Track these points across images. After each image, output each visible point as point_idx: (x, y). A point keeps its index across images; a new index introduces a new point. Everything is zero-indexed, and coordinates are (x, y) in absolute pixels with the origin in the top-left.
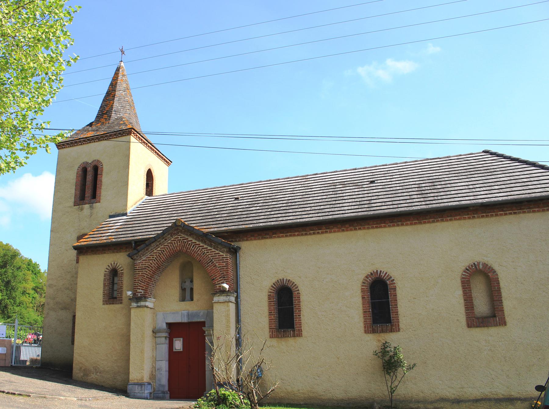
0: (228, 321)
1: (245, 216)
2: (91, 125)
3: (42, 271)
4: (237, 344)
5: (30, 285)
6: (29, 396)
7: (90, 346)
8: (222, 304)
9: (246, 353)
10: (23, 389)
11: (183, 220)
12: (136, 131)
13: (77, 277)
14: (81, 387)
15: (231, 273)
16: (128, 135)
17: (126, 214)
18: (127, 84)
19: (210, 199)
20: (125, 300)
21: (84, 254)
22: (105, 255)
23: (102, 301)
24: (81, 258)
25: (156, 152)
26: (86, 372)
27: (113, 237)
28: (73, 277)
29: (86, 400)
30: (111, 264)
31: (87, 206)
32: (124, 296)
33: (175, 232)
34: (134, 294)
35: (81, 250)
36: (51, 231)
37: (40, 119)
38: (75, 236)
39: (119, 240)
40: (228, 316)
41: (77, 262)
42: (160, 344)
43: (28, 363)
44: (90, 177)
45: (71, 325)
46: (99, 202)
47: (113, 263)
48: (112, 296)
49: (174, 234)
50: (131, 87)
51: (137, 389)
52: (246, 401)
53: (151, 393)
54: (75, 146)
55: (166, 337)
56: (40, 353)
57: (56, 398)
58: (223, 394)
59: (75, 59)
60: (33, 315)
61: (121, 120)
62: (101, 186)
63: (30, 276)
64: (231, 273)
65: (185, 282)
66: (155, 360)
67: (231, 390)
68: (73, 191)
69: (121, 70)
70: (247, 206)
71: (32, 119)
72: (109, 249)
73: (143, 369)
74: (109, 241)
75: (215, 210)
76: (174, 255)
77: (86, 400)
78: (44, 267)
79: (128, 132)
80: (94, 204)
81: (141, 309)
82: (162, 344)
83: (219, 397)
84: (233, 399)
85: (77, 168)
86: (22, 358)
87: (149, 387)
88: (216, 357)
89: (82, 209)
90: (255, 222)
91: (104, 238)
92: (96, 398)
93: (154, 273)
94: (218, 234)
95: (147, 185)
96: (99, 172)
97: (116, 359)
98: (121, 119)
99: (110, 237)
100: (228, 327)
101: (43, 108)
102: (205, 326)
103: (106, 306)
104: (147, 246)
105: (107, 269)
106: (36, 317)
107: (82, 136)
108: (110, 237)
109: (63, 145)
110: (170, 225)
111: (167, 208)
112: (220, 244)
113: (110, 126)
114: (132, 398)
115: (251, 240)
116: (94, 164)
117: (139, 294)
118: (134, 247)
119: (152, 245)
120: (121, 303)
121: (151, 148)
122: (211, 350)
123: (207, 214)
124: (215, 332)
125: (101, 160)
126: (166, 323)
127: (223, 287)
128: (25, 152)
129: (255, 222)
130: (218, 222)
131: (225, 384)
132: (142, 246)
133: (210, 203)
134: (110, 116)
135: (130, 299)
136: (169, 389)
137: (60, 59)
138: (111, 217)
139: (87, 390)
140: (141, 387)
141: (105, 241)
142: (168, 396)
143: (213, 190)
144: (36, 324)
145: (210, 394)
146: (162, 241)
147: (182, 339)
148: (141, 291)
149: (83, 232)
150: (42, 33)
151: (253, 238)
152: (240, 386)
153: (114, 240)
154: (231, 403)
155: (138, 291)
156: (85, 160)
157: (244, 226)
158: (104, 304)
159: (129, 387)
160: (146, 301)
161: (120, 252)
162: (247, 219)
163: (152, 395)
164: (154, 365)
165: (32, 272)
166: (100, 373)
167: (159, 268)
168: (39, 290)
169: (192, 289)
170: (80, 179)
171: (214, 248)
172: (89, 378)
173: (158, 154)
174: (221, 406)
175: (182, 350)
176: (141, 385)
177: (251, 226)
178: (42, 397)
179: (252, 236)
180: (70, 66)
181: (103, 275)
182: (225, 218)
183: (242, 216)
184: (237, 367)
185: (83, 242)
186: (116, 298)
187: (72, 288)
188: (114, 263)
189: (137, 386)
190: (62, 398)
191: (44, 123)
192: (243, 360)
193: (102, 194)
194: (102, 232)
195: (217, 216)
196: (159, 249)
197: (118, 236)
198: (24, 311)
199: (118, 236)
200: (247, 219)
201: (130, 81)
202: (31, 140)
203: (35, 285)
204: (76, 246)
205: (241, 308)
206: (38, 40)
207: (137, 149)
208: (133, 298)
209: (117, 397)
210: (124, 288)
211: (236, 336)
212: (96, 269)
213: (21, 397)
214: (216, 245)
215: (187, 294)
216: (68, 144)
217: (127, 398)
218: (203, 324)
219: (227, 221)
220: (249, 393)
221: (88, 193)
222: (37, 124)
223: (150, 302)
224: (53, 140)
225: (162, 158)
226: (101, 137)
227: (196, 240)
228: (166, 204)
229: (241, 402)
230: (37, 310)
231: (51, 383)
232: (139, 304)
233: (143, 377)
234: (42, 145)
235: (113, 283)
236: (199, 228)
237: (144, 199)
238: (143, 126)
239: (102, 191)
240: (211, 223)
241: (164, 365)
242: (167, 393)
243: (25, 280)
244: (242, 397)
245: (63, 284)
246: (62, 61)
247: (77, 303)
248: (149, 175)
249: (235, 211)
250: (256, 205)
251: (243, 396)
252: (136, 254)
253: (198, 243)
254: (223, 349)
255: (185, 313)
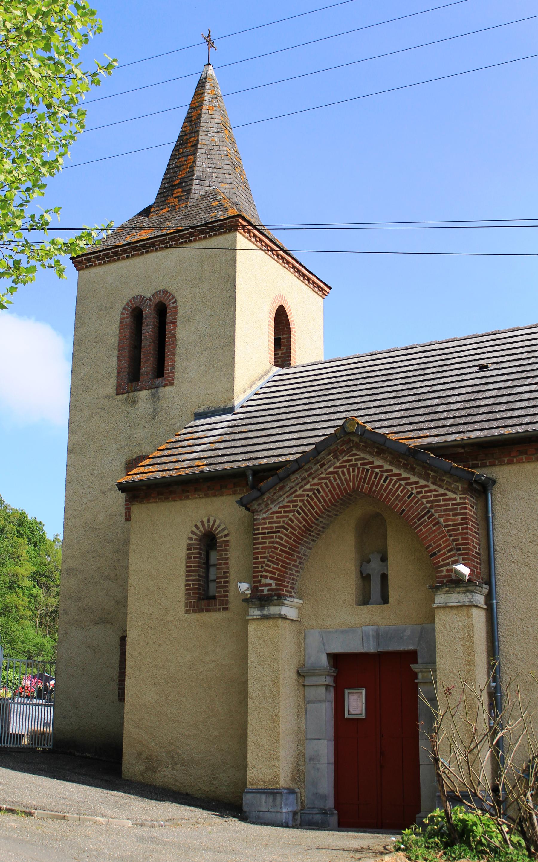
0: (470, 651)
1: (504, 407)
2: (146, 212)
3: (50, 536)
4: (491, 705)
5: (26, 569)
6: (31, 814)
7: (155, 710)
8: (455, 611)
9: (513, 725)
10: (18, 799)
11: (360, 420)
12: (250, 224)
13: (127, 553)
14: (141, 796)
15: (475, 539)
16: (230, 231)
17: (230, 410)
18: (223, 116)
19: (421, 369)
20: (235, 603)
21: (142, 502)
22: (188, 502)
23: (183, 605)
24: (137, 510)
25: (294, 267)
26: (152, 763)
27: (205, 462)
28: (118, 551)
29: (152, 826)
30: (202, 522)
31: (144, 394)
32: (231, 594)
33: (344, 447)
34: (254, 589)
35: (136, 493)
36: (69, 451)
37: (38, 204)
38: (120, 461)
39: (219, 467)
40: (469, 637)
41: (128, 518)
42: (314, 702)
43: (25, 741)
44: (149, 330)
45: (116, 658)
46: (172, 384)
47: (205, 520)
48: (205, 593)
49: (342, 452)
50: (233, 121)
51: (264, 804)
52: (515, 839)
53: (295, 813)
54: (114, 261)
55: (327, 686)
56: (50, 719)
57: (87, 820)
58: (460, 820)
59: (108, 67)
60: (31, 635)
61: (214, 199)
62: (174, 348)
63: (25, 550)
64: (475, 539)
65: (369, 561)
66: (303, 738)
67: (479, 812)
68: (114, 362)
69: (208, 86)
70: (509, 384)
71: (21, 205)
72: (196, 490)
73: (277, 759)
74: (197, 470)
75: (433, 395)
76: (344, 500)
77: (152, 826)
78: (53, 528)
79: (231, 225)
80: (161, 390)
81: (271, 622)
82: (320, 701)
83: (452, 827)
84: (485, 832)
85: (120, 310)
86: (14, 729)
87: (292, 797)
88: (442, 736)
89: (134, 402)
90: (528, 420)
91: (185, 464)
92: (173, 822)
93: (298, 541)
94: (442, 450)
95: (278, 343)
96: (169, 318)
97: (216, 733)
98: (214, 195)
99: (197, 463)
100: (470, 663)
101: (43, 181)
102: (416, 663)
103: (193, 617)
104: (281, 480)
105: (192, 532)
106: (39, 640)
107: (129, 239)
108: (197, 463)
109: (89, 260)
110: (332, 431)
111: (323, 393)
112: (449, 472)
113: (190, 212)
114: (254, 823)
115: (520, 462)
116: (157, 300)
117: (266, 589)
118: (253, 483)
119: (293, 477)
120: (226, 609)
121: (283, 258)
122: (432, 718)
123: (416, 405)
124: (439, 675)
125: (172, 290)
126: (328, 654)
127: (457, 572)
128: (11, 279)
129: (528, 420)
130: (440, 423)
131: (465, 796)
132: (270, 480)
133: (421, 378)
134: (189, 192)
135: (245, 600)
136: (337, 805)
137: (76, 71)
138: (198, 416)
139: (153, 804)
140: (274, 800)
141: (188, 471)
142: (334, 820)
143: (428, 349)
144: (38, 655)
145: (432, 819)
146: (315, 468)
147: (363, 691)
148: (268, 583)
149: (137, 452)
150: (36, 18)
151: (524, 457)
152: (500, 803)
153: (206, 468)
154: (480, 843)
155: (264, 581)
156: (137, 291)
157: (501, 431)
158: (187, 612)
159: (247, 798)
160: (282, 604)
161: (222, 495)
162: (510, 414)
163: (298, 817)
164: (302, 749)
165: (30, 540)
166: (182, 765)
167: (308, 529)
168: (43, 579)
169: (384, 578)
170: (127, 333)
171: (434, 483)
172: (159, 775)
173: (299, 271)
174: (456, 847)
175: (364, 716)
176: (273, 793)
177: (519, 429)
178: (58, 818)
179: (521, 453)
180: (99, 83)
181: (185, 547)
182: (457, 414)
183: (497, 408)
184: (493, 757)
185: (139, 475)
186: (214, 598)
187: (118, 576)
188: (209, 521)
189: (264, 797)
190: (100, 819)
191: (47, 212)
192: (506, 743)
193: (177, 367)
194: (180, 451)
195: (440, 408)
196: (308, 487)
197: (217, 460)
198: (12, 625)
199: (217, 460)
200: (510, 414)
201: (232, 110)
202: (22, 252)
203: (34, 569)
204: (124, 483)
205: (500, 621)
206: (28, 33)
207: (251, 262)
208: (252, 597)
209: (220, 820)
210: (233, 575)
211: (489, 686)
212: (172, 530)
213: (13, 817)
214: (439, 476)
215: (373, 588)
216: (98, 258)
217: (243, 824)
218: (412, 656)
219: (462, 420)
220: (521, 821)
221: (147, 366)
222: (33, 217)
223: (291, 606)
224: (68, 247)
225: (309, 279)
226: (171, 239)
227: (391, 463)
228: (323, 382)
229: (505, 840)
230: (41, 623)
231: (75, 785)
232: (266, 612)
233: (276, 778)
234: (47, 262)
235: (207, 565)
236: (397, 436)
237: (271, 374)
238: (263, 214)
239: (177, 359)
240: (426, 425)
241: (324, 750)
242: (332, 814)
243: (15, 558)
244: (505, 829)
245: (98, 568)
246: (80, 75)
247: (129, 610)
248: (281, 320)
249: (479, 396)
250: (529, 381)
251: (508, 826)
252: (256, 499)
253: (396, 471)
254: (460, 714)
255: (371, 630)
